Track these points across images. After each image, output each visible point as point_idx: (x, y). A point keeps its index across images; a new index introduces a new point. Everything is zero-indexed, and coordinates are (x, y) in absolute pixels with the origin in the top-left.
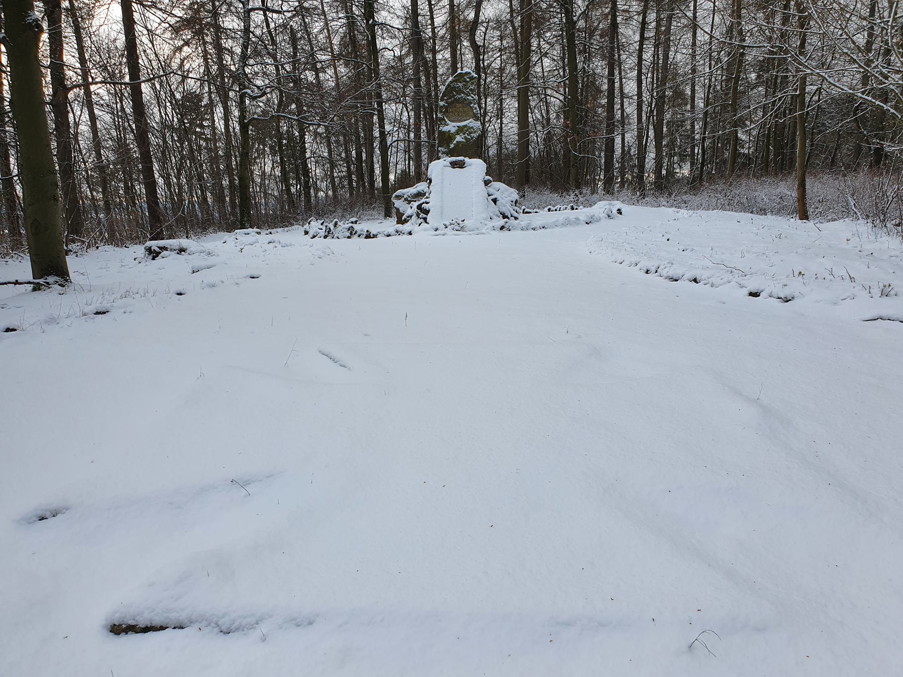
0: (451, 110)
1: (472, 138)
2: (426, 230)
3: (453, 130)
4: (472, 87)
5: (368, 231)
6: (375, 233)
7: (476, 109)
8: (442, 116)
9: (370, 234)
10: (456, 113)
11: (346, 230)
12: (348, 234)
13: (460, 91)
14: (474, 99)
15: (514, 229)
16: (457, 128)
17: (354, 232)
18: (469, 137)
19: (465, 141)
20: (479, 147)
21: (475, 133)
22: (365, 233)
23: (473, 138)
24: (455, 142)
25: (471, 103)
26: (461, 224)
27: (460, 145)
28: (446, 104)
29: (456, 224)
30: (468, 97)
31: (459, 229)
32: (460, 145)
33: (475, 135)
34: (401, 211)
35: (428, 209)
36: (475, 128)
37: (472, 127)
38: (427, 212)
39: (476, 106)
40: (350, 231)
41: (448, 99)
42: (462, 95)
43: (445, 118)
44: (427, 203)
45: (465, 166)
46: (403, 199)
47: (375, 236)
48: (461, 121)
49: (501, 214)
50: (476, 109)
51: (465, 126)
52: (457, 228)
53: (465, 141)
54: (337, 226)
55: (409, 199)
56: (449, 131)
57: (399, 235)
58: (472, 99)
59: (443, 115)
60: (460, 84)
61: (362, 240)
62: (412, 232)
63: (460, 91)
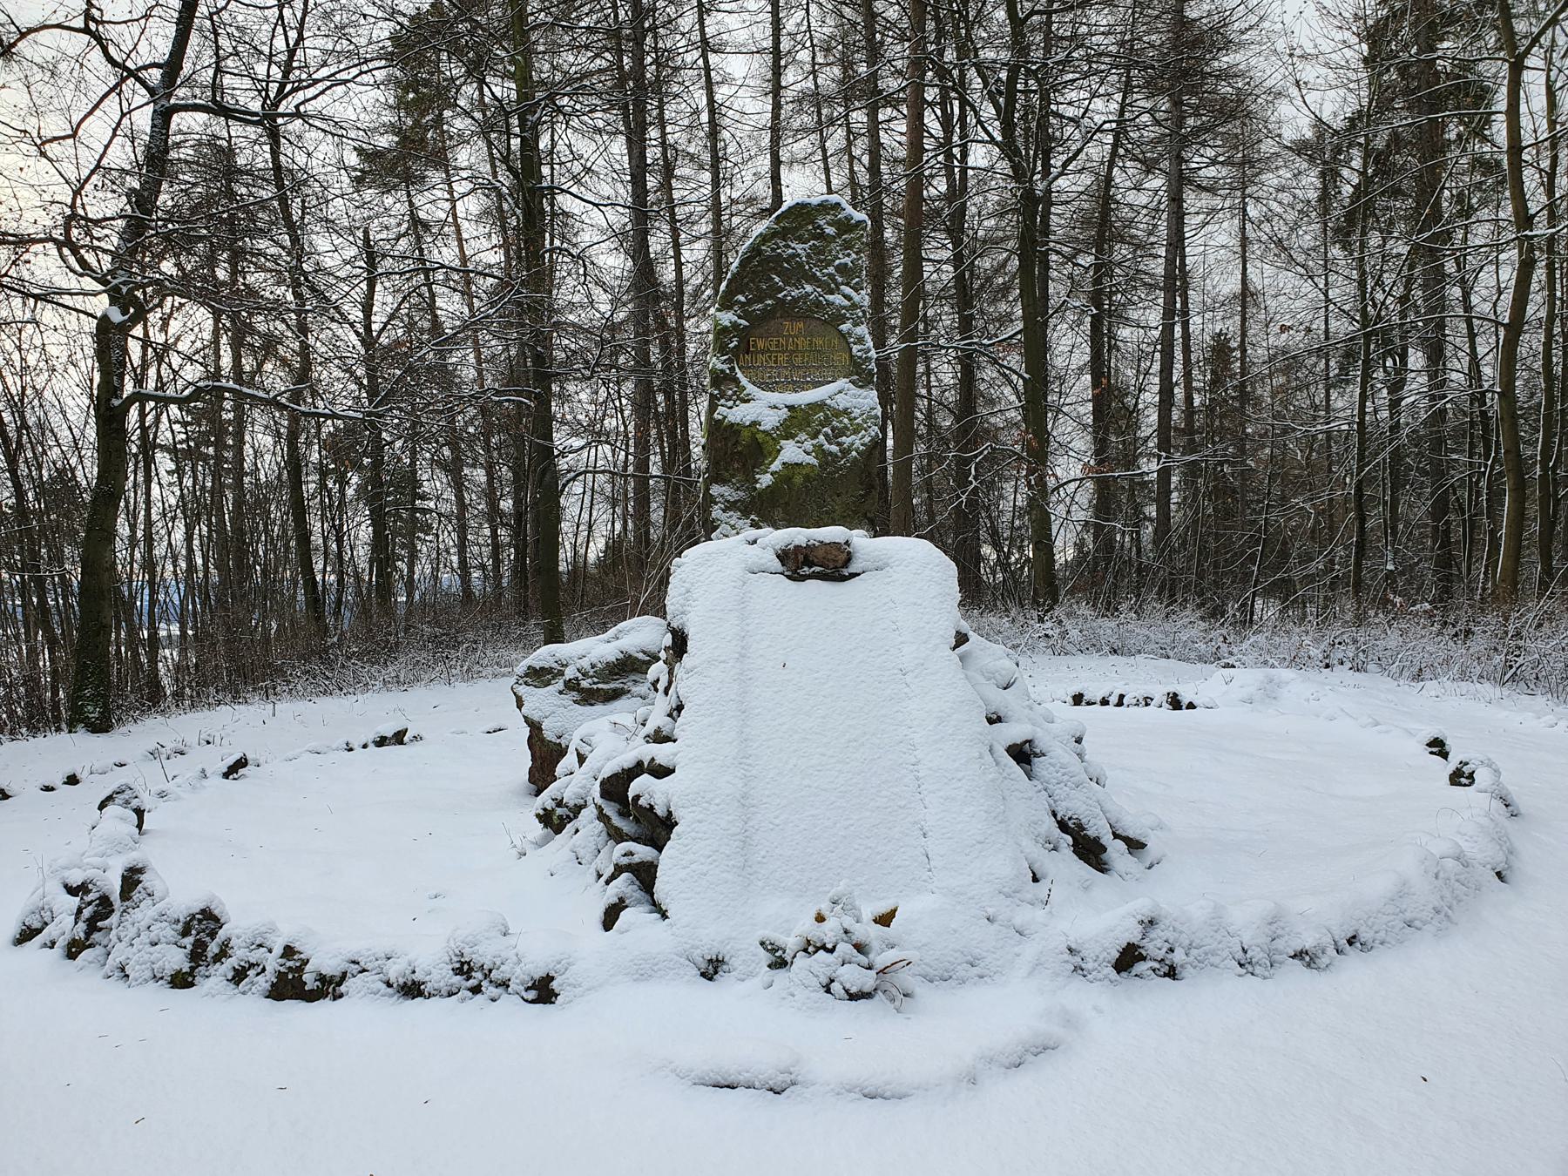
0: (760, 344)
1: (845, 452)
2: (645, 971)
3: (770, 420)
4: (847, 260)
5: (289, 952)
6: (331, 967)
7: (860, 340)
8: (725, 367)
9: (300, 969)
10: (782, 358)
11: (169, 932)
12: (177, 959)
13: (798, 274)
14: (854, 306)
15: (1200, 963)
16: (784, 413)
17: (213, 948)
18: (834, 448)
19: (816, 462)
20: (870, 487)
21: (855, 432)
22: (273, 963)
23: (849, 450)
24: (776, 466)
25: (843, 319)
26: (875, 945)
27: (798, 480)
28: (743, 322)
29: (844, 949)
30: (830, 298)
31: (868, 980)
32: (798, 480)
33: (857, 441)
34: (549, 735)
35: (660, 811)
36: (857, 412)
37: (846, 412)
38: (658, 828)
39: (863, 330)
40: (189, 941)
41: (749, 302)
42: (809, 288)
43: (740, 375)
44: (661, 772)
45: (853, 569)
46: (560, 685)
47: (329, 987)
48: (798, 387)
49: (1063, 826)
50: (860, 340)
51: (819, 406)
52: (855, 977)
53: (816, 462)
54: (136, 896)
55: (585, 684)
56: (755, 423)
57: (476, 990)
58: (846, 303)
59: (729, 361)
60: (799, 248)
61: (252, 1005)
62: (554, 985)
63: (798, 274)
